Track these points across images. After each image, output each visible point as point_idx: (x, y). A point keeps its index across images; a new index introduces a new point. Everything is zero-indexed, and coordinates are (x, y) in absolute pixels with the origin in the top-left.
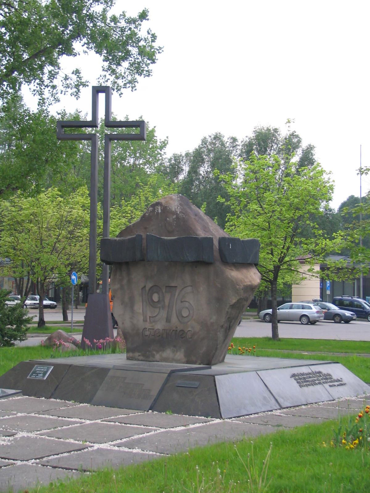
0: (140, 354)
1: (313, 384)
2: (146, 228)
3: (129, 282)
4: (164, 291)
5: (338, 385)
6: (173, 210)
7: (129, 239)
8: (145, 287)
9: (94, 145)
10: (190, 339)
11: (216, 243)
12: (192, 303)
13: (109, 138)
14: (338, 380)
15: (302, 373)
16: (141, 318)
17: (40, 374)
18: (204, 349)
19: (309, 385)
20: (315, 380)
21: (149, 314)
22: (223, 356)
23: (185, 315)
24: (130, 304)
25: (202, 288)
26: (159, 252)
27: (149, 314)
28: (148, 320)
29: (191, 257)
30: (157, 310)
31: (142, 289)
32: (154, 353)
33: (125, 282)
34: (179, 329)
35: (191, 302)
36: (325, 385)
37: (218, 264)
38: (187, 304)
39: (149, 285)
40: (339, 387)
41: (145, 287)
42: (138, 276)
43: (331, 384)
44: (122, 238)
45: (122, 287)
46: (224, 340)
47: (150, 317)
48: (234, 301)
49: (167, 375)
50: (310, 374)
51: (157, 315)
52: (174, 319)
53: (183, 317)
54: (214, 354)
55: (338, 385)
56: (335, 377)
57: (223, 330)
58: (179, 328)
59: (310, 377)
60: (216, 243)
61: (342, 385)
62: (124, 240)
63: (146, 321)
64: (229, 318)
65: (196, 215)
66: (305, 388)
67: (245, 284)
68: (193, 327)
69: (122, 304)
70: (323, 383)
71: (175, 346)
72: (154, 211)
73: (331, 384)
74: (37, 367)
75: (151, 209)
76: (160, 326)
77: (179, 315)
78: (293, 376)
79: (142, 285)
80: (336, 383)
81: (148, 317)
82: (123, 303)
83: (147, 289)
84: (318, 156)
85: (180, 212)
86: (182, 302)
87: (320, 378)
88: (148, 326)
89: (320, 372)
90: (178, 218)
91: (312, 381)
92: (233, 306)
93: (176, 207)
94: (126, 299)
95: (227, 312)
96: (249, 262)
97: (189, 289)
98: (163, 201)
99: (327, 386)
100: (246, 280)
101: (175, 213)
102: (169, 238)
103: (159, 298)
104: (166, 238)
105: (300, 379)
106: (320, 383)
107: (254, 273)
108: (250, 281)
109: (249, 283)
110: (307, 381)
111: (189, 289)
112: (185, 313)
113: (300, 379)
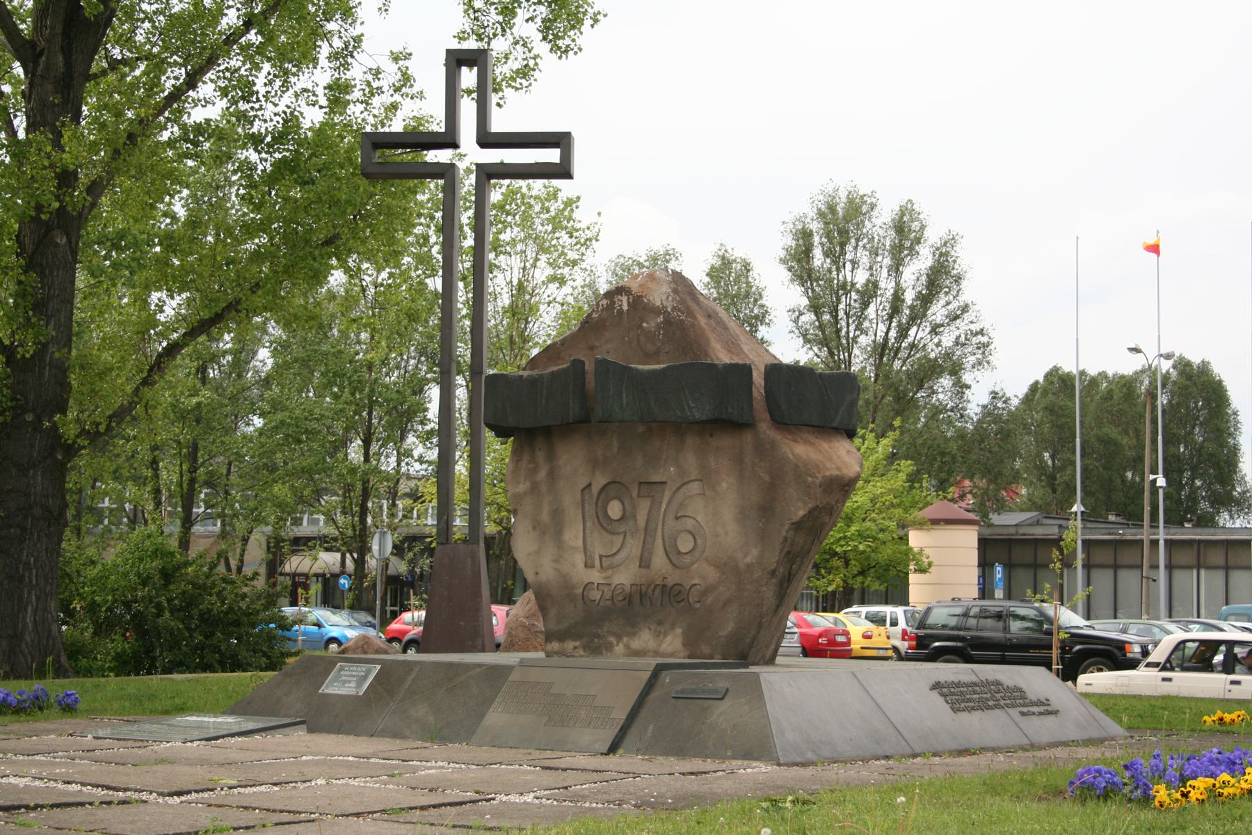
0: (577, 644)
1: (983, 706)
2: (592, 348)
3: (552, 475)
4: (635, 494)
5: (1040, 714)
6: (658, 303)
7: (553, 373)
8: (590, 485)
9: (450, 190)
10: (698, 605)
11: (758, 378)
12: (707, 516)
13: (487, 173)
14: (1039, 703)
15: (956, 681)
16: (579, 559)
17: (349, 682)
18: (730, 627)
19: (973, 709)
20: (987, 699)
21: (598, 550)
22: (772, 647)
23: (683, 549)
24: (553, 529)
25: (727, 484)
26: (625, 401)
27: (598, 550)
28: (597, 563)
29: (699, 410)
30: (620, 539)
31: (583, 490)
32: (612, 639)
33: (542, 475)
34: (670, 582)
35: (699, 519)
36: (1011, 711)
37: (765, 428)
38: (689, 523)
39: (600, 481)
40: (1042, 717)
41: (590, 485)
42: (574, 462)
43: (1025, 710)
44: (535, 373)
45: (534, 488)
46: (778, 606)
47: (601, 557)
48: (801, 513)
49: (649, 673)
50: (975, 684)
51: (619, 551)
52: (659, 560)
53: (679, 553)
54: (754, 639)
55: (1040, 714)
56: (1032, 696)
57: (774, 580)
58: (670, 579)
59: (975, 693)
60: (758, 378)
61: (1050, 713)
62: (541, 376)
63: (593, 567)
64: (789, 553)
65: (709, 316)
66: (964, 716)
67: (828, 474)
68: (702, 574)
69: (534, 528)
70: (1007, 705)
71: (660, 623)
72: (611, 307)
73: (1025, 710)
74: (342, 669)
75: (605, 302)
76: (625, 578)
77: (671, 551)
78: (937, 686)
79: (583, 482)
80: (1035, 709)
81: (597, 557)
82: (536, 525)
83: (595, 489)
84: (965, 258)
85: (674, 308)
86: (677, 518)
87: (998, 696)
88: (595, 576)
89: (998, 683)
90: (668, 322)
91: (980, 700)
92: (798, 526)
93: (664, 298)
94: (545, 516)
95: (786, 539)
96: (835, 425)
97: (695, 487)
98: (635, 288)
99: (1014, 712)
100: (828, 465)
101: (657, 311)
102: (647, 367)
103: (624, 510)
104: (640, 367)
105: (954, 694)
106: (997, 707)
107: (848, 452)
108: (838, 469)
109: (836, 473)
110: (969, 700)
111: (695, 487)
112: (685, 544)
113: (954, 694)
